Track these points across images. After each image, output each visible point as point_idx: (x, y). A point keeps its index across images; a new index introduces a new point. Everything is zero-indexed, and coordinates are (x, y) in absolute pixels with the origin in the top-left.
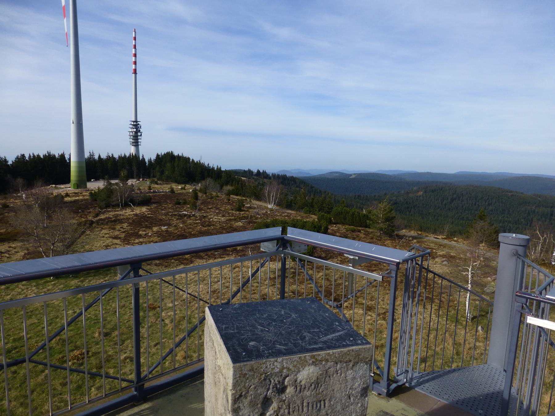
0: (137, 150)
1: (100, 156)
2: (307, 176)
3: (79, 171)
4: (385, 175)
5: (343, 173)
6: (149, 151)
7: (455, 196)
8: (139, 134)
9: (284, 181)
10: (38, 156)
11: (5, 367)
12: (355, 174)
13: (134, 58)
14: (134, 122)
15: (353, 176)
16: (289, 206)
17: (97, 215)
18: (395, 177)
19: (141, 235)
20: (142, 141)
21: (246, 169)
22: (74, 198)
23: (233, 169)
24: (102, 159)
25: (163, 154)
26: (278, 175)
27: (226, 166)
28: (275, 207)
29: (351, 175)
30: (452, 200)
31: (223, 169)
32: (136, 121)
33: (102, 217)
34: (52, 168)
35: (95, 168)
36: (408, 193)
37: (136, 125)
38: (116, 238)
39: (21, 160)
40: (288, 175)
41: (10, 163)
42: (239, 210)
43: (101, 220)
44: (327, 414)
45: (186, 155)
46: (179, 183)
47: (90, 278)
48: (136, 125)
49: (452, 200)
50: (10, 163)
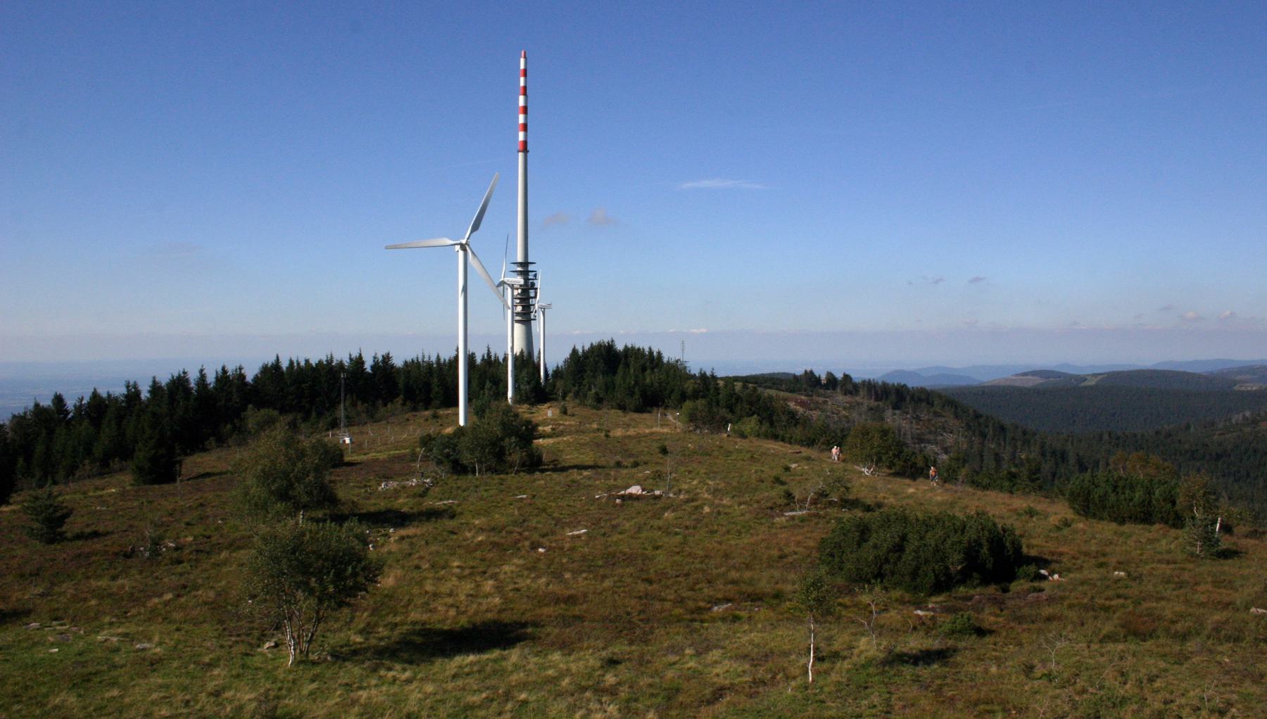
1: (438, 358)
2: (963, 383)
4: (1184, 373)
5: (1065, 375)
8: (532, 293)
12: (1095, 375)
14: (521, 264)
15: (1092, 382)
18: (1209, 379)
21: (799, 371)
23: (753, 373)
24: (392, 366)
25: (586, 348)
29: (1084, 379)
39: (272, 372)
40: (912, 384)
41: (249, 378)
45: (643, 344)
47: (439, 626)
48: (476, 227)
50: (249, 378)
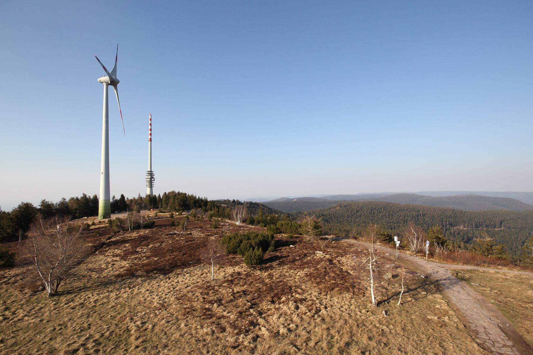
0: (151, 191)
3: (106, 207)
5: (288, 199)
6: (159, 191)
7: (358, 209)
9: (252, 206)
10: (77, 199)
11: (256, 222)
13: (150, 127)
15: (295, 200)
16: (252, 222)
17: (110, 238)
19: (137, 252)
20: (155, 184)
22: (98, 226)
26: (247, 202)
27: (211, 197)
28: (241, 224)
29: (293, 199)
30: (357, 211)
31: (208, 200)
32: (151, 171)
33: (113, 239)
34: (88, 206)
35: (120, 205)
36: (330, 209)
37: (151, 174)
38: (117, 256)
39: (234, 201)
42: (216, 227)
43: (112, 241)
44: (264, 354)
46: (177, 211)
49: (357, 211)
